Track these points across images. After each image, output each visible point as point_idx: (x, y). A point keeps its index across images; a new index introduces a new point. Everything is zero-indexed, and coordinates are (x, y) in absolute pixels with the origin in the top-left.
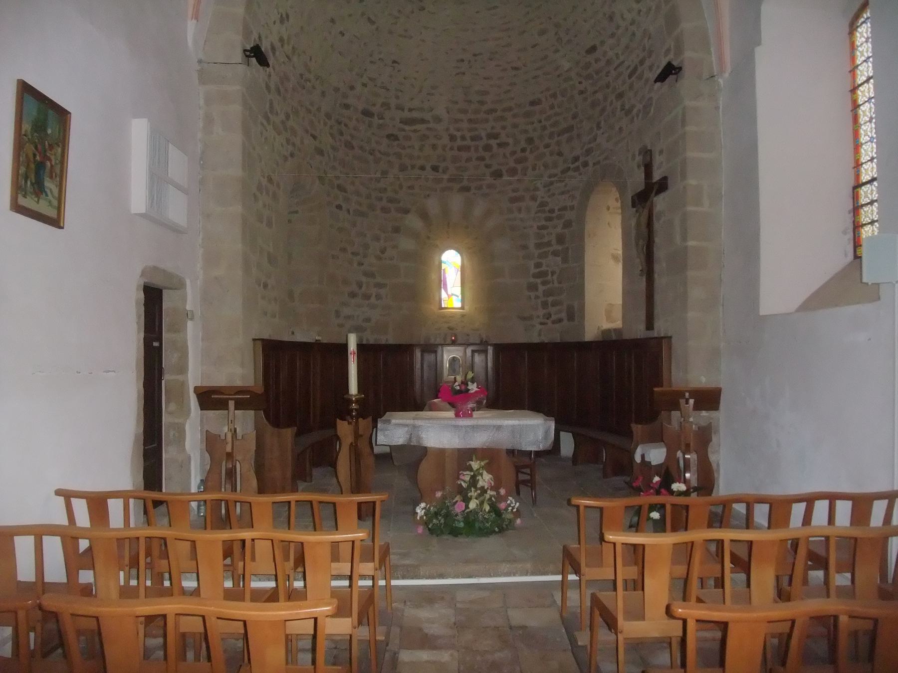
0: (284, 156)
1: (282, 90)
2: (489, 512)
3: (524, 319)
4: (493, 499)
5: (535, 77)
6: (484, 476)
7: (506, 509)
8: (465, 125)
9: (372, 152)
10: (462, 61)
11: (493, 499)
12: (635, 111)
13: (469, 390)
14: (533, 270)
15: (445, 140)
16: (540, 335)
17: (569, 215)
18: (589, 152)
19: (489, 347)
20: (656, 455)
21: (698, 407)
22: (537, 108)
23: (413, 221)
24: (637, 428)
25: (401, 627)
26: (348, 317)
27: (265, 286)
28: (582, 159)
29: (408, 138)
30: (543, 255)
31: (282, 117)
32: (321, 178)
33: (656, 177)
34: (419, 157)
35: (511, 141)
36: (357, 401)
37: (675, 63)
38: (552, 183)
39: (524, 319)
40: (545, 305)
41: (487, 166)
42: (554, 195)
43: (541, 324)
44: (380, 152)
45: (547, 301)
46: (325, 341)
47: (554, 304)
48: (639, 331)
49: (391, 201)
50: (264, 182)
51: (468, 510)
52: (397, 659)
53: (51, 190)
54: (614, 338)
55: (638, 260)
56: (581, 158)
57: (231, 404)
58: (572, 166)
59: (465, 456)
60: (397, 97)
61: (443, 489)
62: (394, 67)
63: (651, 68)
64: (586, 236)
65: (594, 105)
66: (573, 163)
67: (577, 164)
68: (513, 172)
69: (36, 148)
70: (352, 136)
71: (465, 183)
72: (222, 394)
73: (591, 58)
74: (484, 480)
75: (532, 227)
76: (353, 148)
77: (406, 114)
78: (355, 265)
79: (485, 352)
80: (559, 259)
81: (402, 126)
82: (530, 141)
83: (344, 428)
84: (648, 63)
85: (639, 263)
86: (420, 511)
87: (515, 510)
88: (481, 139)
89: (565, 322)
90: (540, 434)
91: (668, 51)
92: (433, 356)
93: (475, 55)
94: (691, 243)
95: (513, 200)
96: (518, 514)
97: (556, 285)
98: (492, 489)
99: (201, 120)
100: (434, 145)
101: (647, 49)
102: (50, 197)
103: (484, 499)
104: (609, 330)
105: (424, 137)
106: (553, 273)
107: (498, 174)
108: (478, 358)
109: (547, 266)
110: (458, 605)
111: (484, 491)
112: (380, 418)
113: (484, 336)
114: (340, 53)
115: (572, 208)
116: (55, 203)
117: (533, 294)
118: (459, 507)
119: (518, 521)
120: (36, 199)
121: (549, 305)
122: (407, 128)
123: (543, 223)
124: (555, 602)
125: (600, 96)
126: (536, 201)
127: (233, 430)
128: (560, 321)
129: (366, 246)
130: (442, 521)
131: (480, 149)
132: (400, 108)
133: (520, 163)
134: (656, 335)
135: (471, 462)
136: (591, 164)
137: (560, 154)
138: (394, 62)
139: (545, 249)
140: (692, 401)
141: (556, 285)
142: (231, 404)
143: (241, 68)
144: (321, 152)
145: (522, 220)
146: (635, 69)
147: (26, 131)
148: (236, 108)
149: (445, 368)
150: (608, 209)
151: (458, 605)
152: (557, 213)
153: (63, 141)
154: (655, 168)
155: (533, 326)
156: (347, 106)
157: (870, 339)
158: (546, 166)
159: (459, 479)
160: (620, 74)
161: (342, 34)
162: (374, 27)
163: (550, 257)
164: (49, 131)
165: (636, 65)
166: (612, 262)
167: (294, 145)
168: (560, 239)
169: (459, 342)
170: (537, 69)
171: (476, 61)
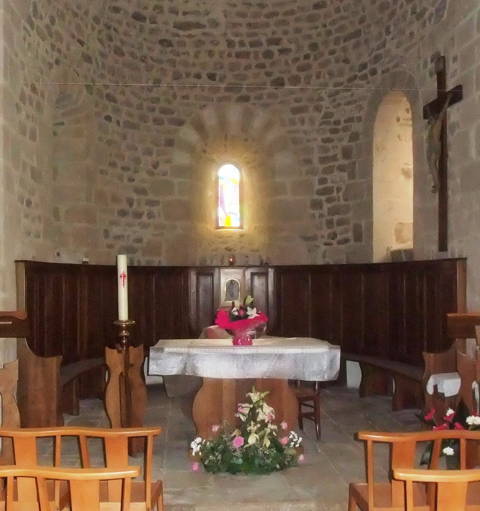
2: (270, 447)
3: (307, 239)
4: (274, 433)
6: (264, 409)
7: (288, 445)
8: (244, 30)
9: (143, 59)
11: (274, 433)
12: (427, 15)
14: (317, 187)
15: (223, 46)
16: (324, 257)
17: (356, 127)
19: (270, 270)
22: (321, 11)
26: (118, 237)
27: (29, 203)
28: (369, 67)
29: (182, 44)
31: (47, 21)
33: (450, 85)
34: (194, 65)
35: (293, 47)
36: (128, 328)
38: (337, 93)
39: (307, 239)
40: (330, 224)
41: (268, 74)
42: (339, 105)
43: (326, 244)
44: (152, 59)
45: (332, 219)
46: (93, 264)
47: (340, 223)
50: (28, 91)
51: (247, 446)
54: (404, 259)
55: (430, 176)
56: (369, 65)
61: (220, 422)
66: (360, 71)
67: (364, 71)
68: (295, 80)
70: (122, 42)
71: (244, 92)
74: (265, 413)
75: (316, 139)
76: (123, 54)
77: (181, 18)
78: (125, 181)
79: (266, 274)
80: (345, 174)
81: (176, 30)
82: (314, 47)
85: (431, 180)
86: (195, 446)
87: (297, 445)
88: (261, 44)
89: (352, 242)
90: (325, 363)
92: (209, 279)
95: (297, 111)
96: (301, 449)
97: (342, 202)
98: (273, 422)
100: (211, 51)
103: (265, 434)
104: (399, 252)
105: (200, 43)
106: (339, 190)
107: (279, 83)
108: (258, 282)
109: (333, 182)
111: (264, 425)
115: (359, 119)
117: (317, 213)
118: (237, 443)
119: (301, 457)
122: (181, 33)
123: (328, 135)
128: (346, 241)
129: (137, 161)
130: (219, 457)
132: (174, 11)
134: (449, 257)
137: (346, 61)
139: (331, 164)
141: (342, 202)
144: (88, 59)
145: (305, 132)
149: (222, 292)
150: (398, 120)
154: (448, 75)
158: (331, 74)
159: (237, 411)
163: (336, 173)
166: (402, 178)
167: (59, 51)
168: (347, 153)
169: (237, 264)
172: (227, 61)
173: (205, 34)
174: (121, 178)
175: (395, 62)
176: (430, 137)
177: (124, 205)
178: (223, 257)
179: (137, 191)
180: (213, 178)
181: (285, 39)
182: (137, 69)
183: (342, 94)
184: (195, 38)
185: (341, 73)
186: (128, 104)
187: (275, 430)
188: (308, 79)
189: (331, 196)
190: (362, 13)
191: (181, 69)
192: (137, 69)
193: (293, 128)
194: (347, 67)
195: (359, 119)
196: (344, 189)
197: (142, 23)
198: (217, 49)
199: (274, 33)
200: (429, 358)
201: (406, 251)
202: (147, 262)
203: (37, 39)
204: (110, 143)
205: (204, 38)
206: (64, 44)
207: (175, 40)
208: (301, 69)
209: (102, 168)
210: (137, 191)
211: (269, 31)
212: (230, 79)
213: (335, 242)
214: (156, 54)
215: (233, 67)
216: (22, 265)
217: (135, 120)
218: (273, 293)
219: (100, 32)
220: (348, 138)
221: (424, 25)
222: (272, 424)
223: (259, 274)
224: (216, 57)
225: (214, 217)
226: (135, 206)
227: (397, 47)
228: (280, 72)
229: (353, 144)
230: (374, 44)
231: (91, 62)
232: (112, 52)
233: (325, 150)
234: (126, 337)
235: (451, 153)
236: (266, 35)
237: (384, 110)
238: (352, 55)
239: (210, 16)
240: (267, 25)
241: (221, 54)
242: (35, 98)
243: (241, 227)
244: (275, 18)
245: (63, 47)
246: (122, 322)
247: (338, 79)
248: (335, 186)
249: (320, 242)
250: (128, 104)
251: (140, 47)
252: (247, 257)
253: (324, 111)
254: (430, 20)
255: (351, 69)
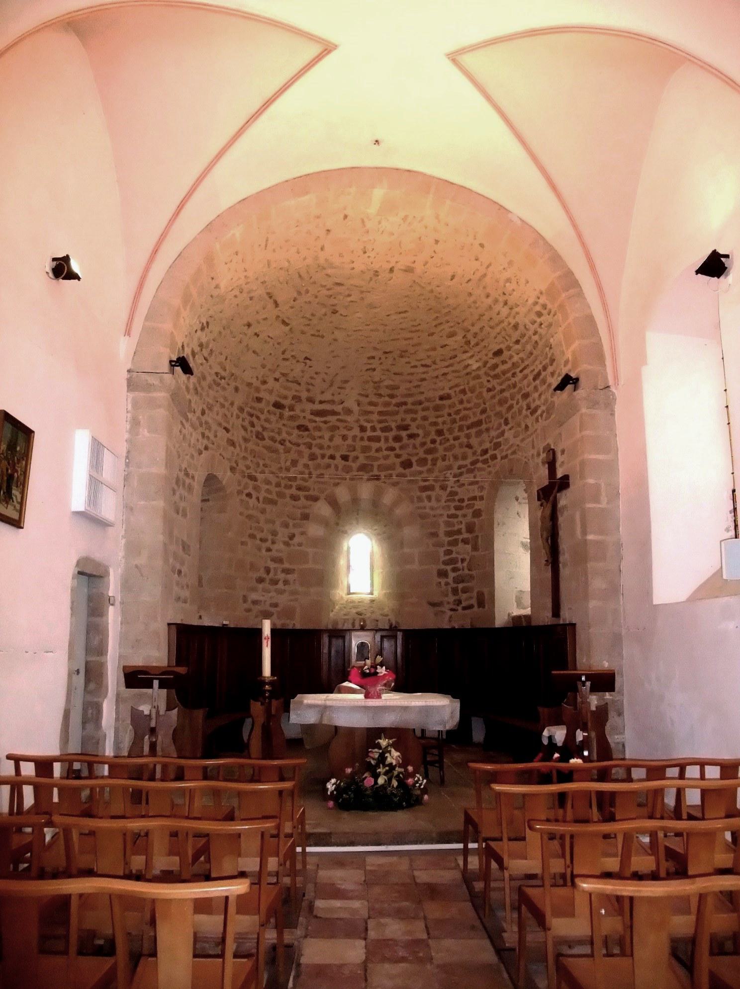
0: (199, 450)
1: (199, 389)
2: (397, 787)
3: (433, 605)
4: (401, 775)
5: (444, 374)
6: (392, 753)
7: (414, 785)
8: (375, 417)
9: (282, 442)
10: (373, 358)
11: (401, 775)
12: (539, 412)
13: (378, 673)
14: (443, 558)
15: (356, 431)
16: (450, 621)
17: (478, 505)
18: (497, 446)
19: (398, 633)
20: (559, 734)
21: (593, 690)
22: (447, 402)
23: (323, 509)
24: (543, 711)
25: (316, 884)
26: (255, 602)
27: (180, 572)
28: (491, 452)
29: (319, 429)
30: (454, 543)
31: (198, 413)
32: (232, 469)
33: (559, 474)
34: (329, 447)
35: (420, 432)
36: (271, 683)
37: (573, 375)
38: (461, 474)
39: (433, 605)
40: (455, 591)
41: (398, 456)
42: (463, 485)
43: (452, 610)
44: (290, 442)
45: (457, 587)
46: (232, 626)
47: (465, 591)
48: (545, 617)
49: (299, 488)
50: (181, 475)
51: (376, 786)
52: (314, 906)
53: (16, 497)
54: (524, 624)
55: (544, 551)
56: (489, 451)
57: (156, 683)
58: (481, 458)
59: (373, 734)
60: (308, 390)
61: (353, 766)
62: (306, 364)
63: (552, 374)
64: (495, 525)
65: (501, 402)
66: (481, 455)
67: (485, 457)
68: (422, 462)
69: (9, 464)
70: (264, 429)
71: (375, 472)
72: (149, 674)
73: (496, 360)
74: (392, 757)
75: (441, 515)
76: (263, 439)
77: (318, 407)
78: (264, 551)
79: (395, 637)
80: (468, 547)
81: (312, 417)
82: (440, 433)
83: (257, 708)
84: (550, 369)
85: (544, 555)
86: (331, 786)
87: (422, 787)
88: (391, 430)
89: (476, 609)
90: (446, 715)
91: (567, 362)
92: (340, 641)
93: (386, 353)
94: (590, 537)
95: (424, 489)
96: (425, 791)
97: (466, 571)
98: (400, 766)
99: (128, 423)
100: (344, 436)
101: (549, 356)
102: (15, 503)
103: (393, 775)
104: (519, 618)
105: (334, 428)
106: (463, 560)
107: (407, 464)
108: (386, 644)
109: (458, 553)
110: (368, 868)
111: (392, 767)
112: (293, 698)
113: (394, 624)
114: (254, 352)
115: (482, 498)
116: (18, 507)
117: (443, 581)
118: (369, 781)
119: (426, 797)
120: (6, 505)
121: (460, 591)
122: (317, 419)
123: (453, 511)
124: (458, 865)
125: (506, 394)
126: (446, 490)
127: (156, 707)
128: (470, 607)
129: (274, 533)
130: (352, 796)
131: (390, 440)
132: (311, 400)
133: (431, 453)
134: (561, 622)
135: (380, 740)
136: (499, 457)
137: (469, 446)
138: (306, 358)
139: (456, 537)
140: (588, 684)
141: (466, 571)
142: (156, 683)
143: (168, 377)
144: (232, 443)
145: (432, 508)
146: (539, 374)
147: (3, 451)
148: (161, 414)
149: (353, 653)
150: (517, 499)
151: (368, 868)
152: (466, 503)
153: (26, 455)
154: (558, 464)
155: (443, 612)
156: (259, 400)
157: (737, 627)
158: (456, 458)
159: (368, 756)
160: (526, 377)
161: (257, 335)
162: (288, 328)
163: (461, 545)
164: (18, 449)
165: (540, 370)
166: (521, 550)
167: (208, 438)
168: (470, 529)
169: (367, 628)
170: (447, 367)
171: (386, 358)
172: (359, 444)
173: (339, 420)
174: (259, 549)
175: (513, 449)
176: (543, 518)
177: (262, 573)
178: (354, 620)
179: (274, 560)
180: (345, 548)
181: (414, 425)
182: (276, 451)
183: (465, 476)
184: (331, 424)
185: (464, 457)
186: (268, 482)
187: (401, 773)
188: (434, 462)
189: (456, 566)
190: (483, 406)
191: (315, 450)
192: (276, 451)
193: (421, 504)
194: (469, 452)
195: (482, 498)
196: (468, 560)
197: (282, 411)
198: (351, 434)
199: (402, 420)
200: (543, 711)
201: (526, 616)
202: (283, 625)
203: (191, 429)
204: (249, 517)
205: (338, 424)
206: (213, 432)
207: (311, 426)
208: (429, 451)
209: (243, 540)
210: (274, 560)
211: (398, 418)
212: (362, 460)
213: (460, 608)
214: (294, 438)
215: (365, 449)
216: (174, 628)
217: (274, 496)
218: (402, 656)
219: (243, 420)
220: (471, 514)
221: (537, 420)
222: (399, 767)
223: (389, 637)
224: (349, 441)
225: (345, 583)
226: (271, 575)
227: (515, 437)
228: (409, 454)
229: (476, 520)
230: (493, 433)
231: (235, 447)
232: (254, 437)
233: (448, 524)
234: (269, 691)
235: (561, 533)
236: (396, 421)
237: (504, 491)
238: (474, 441)
239: (345, 405)
240: (397, 413)
241: (354, 437)
242: (188, 481)
243: (372, 593)
244: (404, 407)
245: (211, 436)
246: (265, 677)
247: (461, 462)
248: (460, 557)
249: (446, 608)
250: (268, 482)
251: (279, 433)
252: (377, 621)
253: (449, 489)
254: (541, 415)
255: (474, 453)
